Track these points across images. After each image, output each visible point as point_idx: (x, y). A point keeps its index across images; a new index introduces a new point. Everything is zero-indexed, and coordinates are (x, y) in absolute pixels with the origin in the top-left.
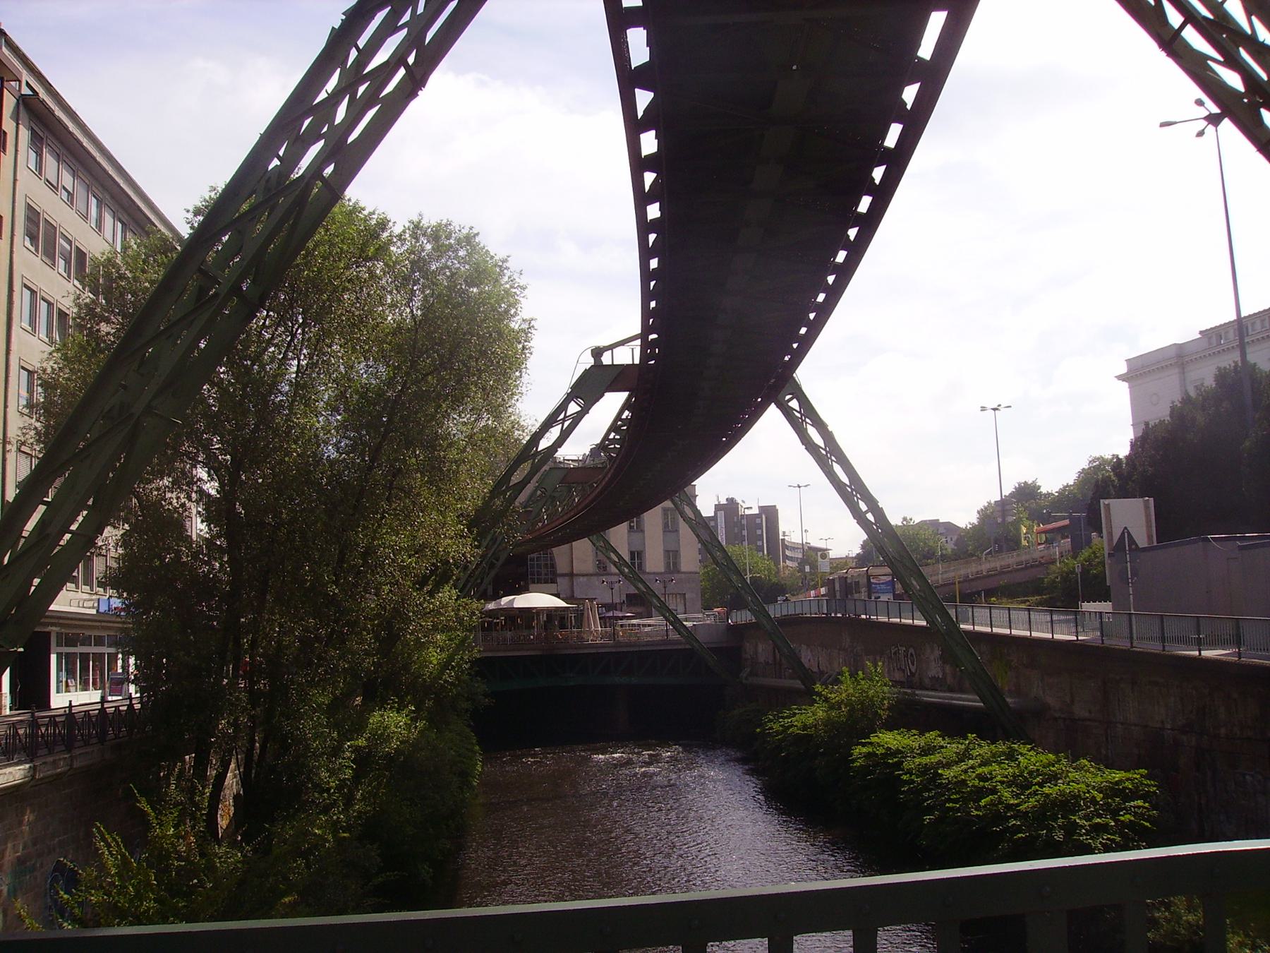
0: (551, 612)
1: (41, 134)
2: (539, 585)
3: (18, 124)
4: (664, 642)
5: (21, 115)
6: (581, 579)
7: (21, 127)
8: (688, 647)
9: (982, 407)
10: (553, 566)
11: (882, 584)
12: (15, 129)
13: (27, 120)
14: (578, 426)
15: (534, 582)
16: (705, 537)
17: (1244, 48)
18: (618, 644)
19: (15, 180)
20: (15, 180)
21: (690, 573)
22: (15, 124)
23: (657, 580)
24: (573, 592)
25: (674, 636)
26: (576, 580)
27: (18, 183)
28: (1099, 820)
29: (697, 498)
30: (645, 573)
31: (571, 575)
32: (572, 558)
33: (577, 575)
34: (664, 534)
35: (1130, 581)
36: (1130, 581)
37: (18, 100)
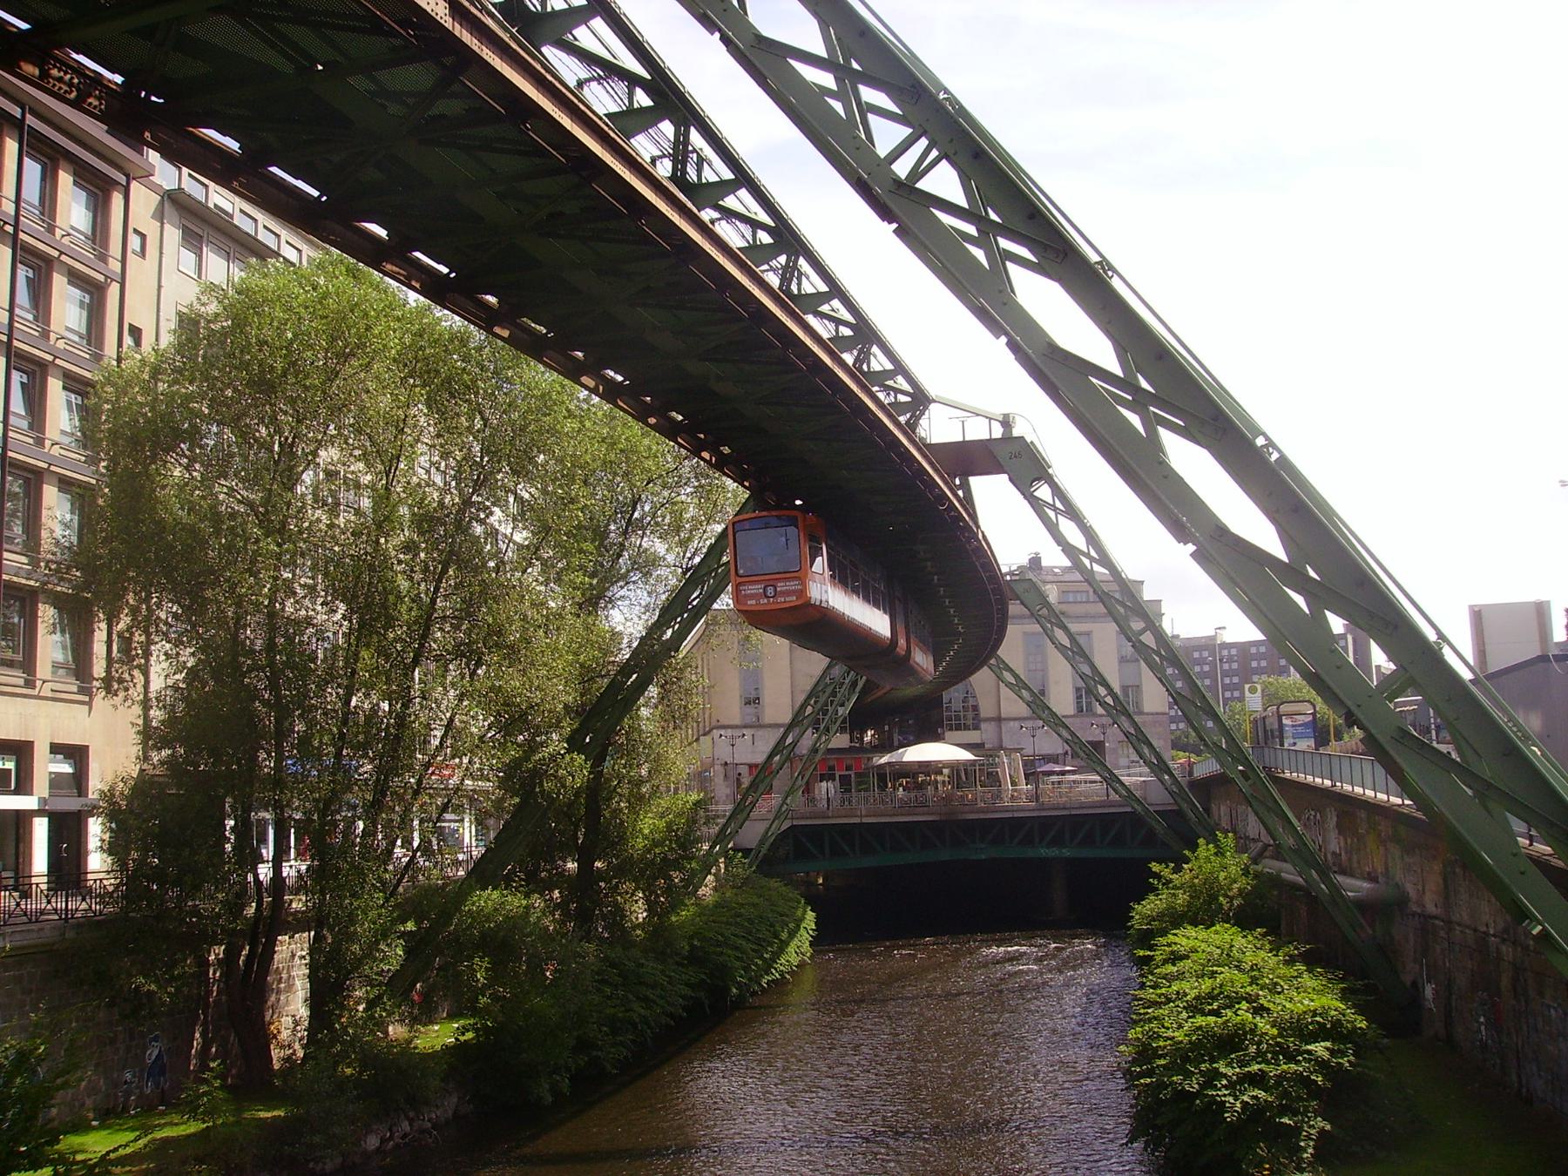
0: (955, 767)
1: (196, 230)
2: (959, 732)
3: (162, 224)
4: (1101, 805)
5: (166, 214)
6: (1012, 723)
7: (167, 226)
8: (1175, 808)
9: (1561, 481)
10: (975, 708)
11: (1299, 726)
12: (159, 229)
13: (176, 219)
14: (1045, 530)
15: (951, 729)
16: (1086, 669)
17: (791, 58)
18: (1042, 808)
19: (160, 287)
20: (160, 287)
21: (1157, 714)
22: (159, 224)
23: (1092, 724)
24: (1001, 740)
25: (1114, 797)
26: (1005, 726)
27: (163, 290)
28: (84, 1084)
29: (1164, 617)
30: (1141, 713)
31: (999, 720)
32: (999, 697)
33: (1005, 719)
34: (1119, 665)
35: (1432, 720)
36: (1432, 720)
37: (162, 197)
